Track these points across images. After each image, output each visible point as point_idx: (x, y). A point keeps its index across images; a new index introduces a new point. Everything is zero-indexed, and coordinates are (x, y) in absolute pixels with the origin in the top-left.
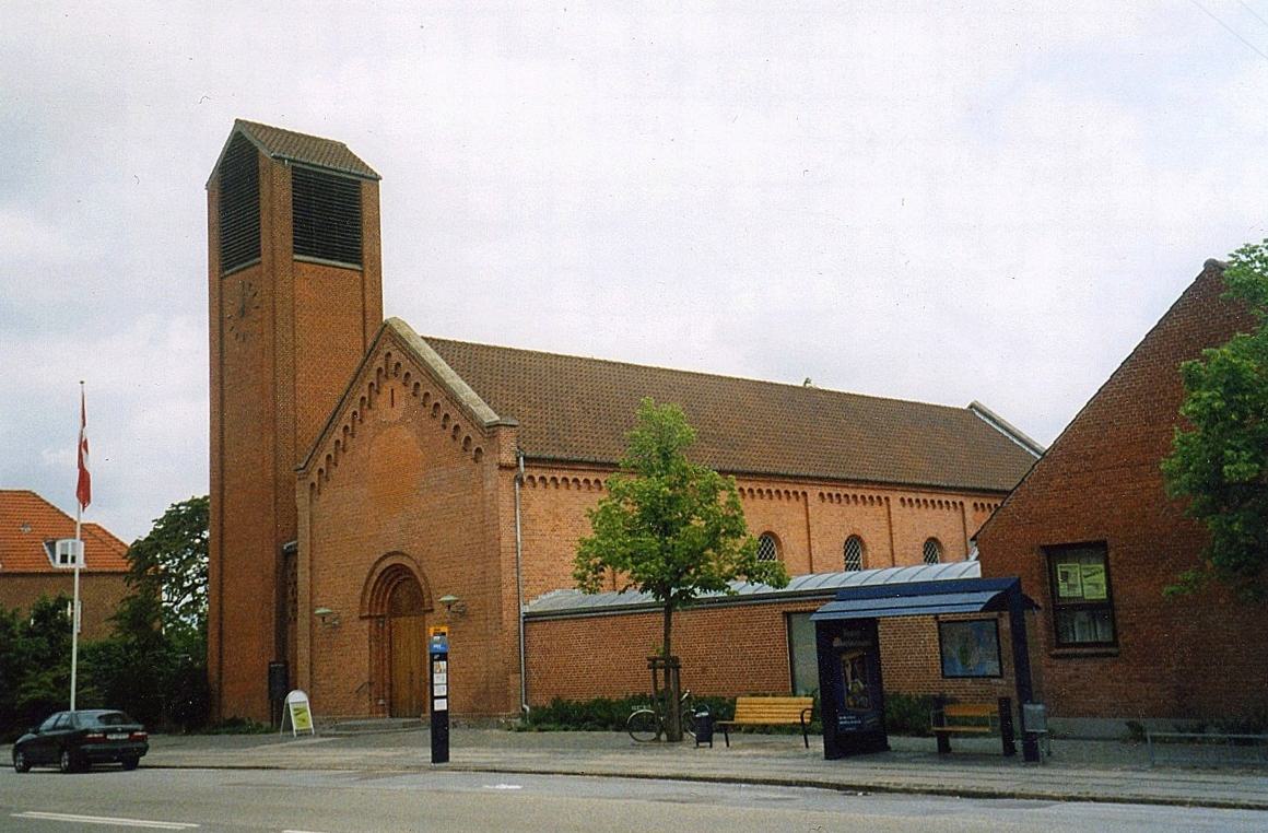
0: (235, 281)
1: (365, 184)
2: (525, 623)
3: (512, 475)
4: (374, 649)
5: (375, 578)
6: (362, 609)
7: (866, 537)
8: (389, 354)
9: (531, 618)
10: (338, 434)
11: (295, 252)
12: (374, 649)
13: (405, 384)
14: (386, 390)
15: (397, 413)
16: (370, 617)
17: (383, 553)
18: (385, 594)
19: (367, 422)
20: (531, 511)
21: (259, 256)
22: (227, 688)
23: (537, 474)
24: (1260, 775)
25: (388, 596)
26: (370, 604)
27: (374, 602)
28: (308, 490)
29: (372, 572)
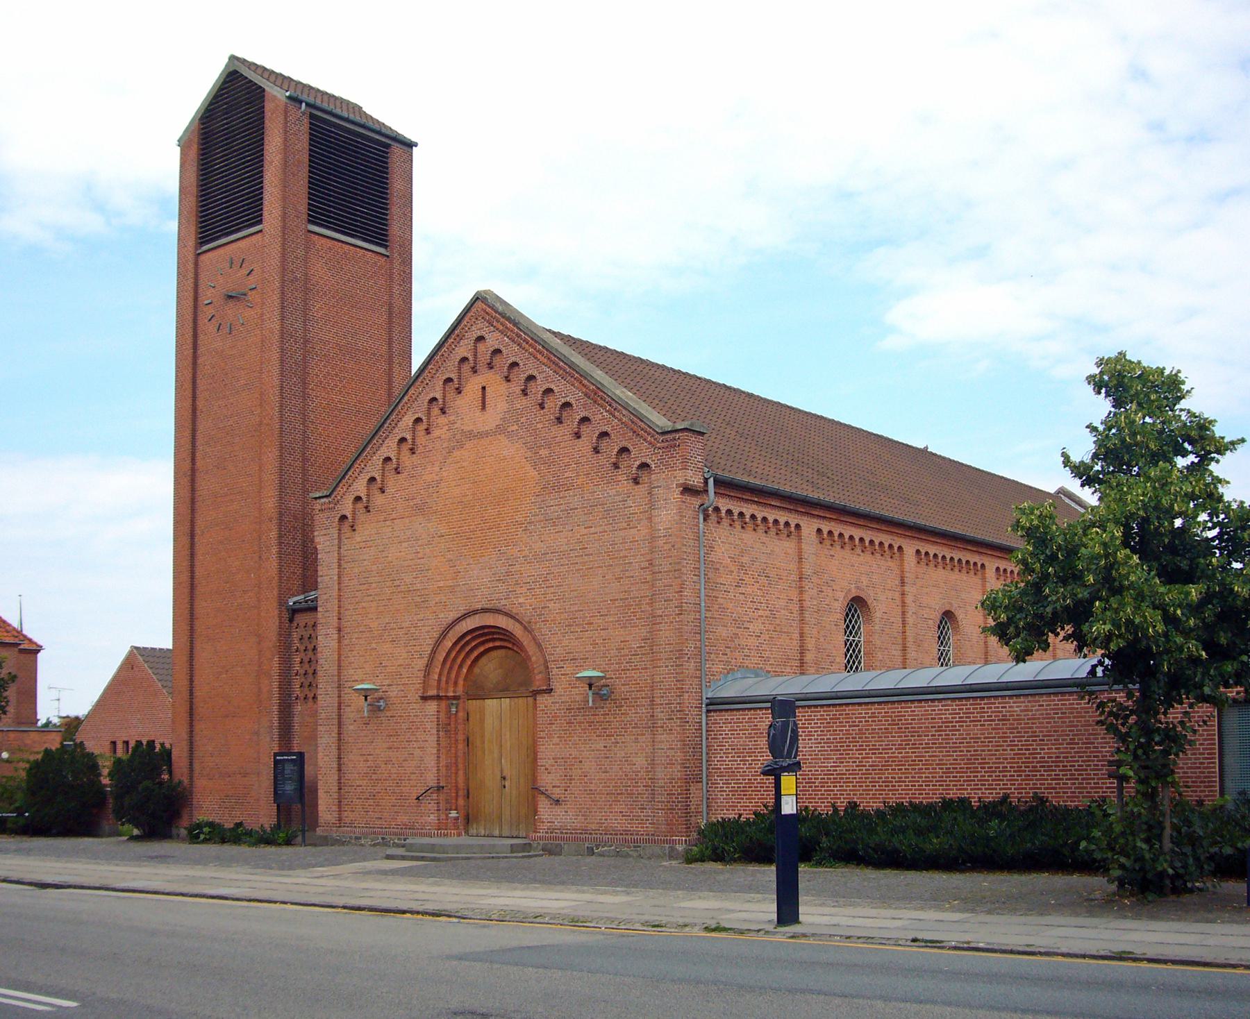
0: (217, 257)
1: (396, 149)
2: (708, 711)
3: (696, 502)
4: (443, 743)
5: (448, 644)
6: (425, 689)
7: (960, 615)
8: (481, 339)
9: (716, 705)
10: (389, 448)
11: (309, 221)
12: (443, 743)
13: (507, 379)
14: (472, 386)
15: (491, 418)
16: (438, 698)
17: (462, 610)
18: (461, 666)
19: (436, 433)
20: (713, 557)
21: (260, 222)
22: (200, 783)
23: (724, 505)
24: (316, 765)
25: (465, 670)
26: (439, 681)
27: (444, 679)
28: (336, 524)
29: (444, 635)
